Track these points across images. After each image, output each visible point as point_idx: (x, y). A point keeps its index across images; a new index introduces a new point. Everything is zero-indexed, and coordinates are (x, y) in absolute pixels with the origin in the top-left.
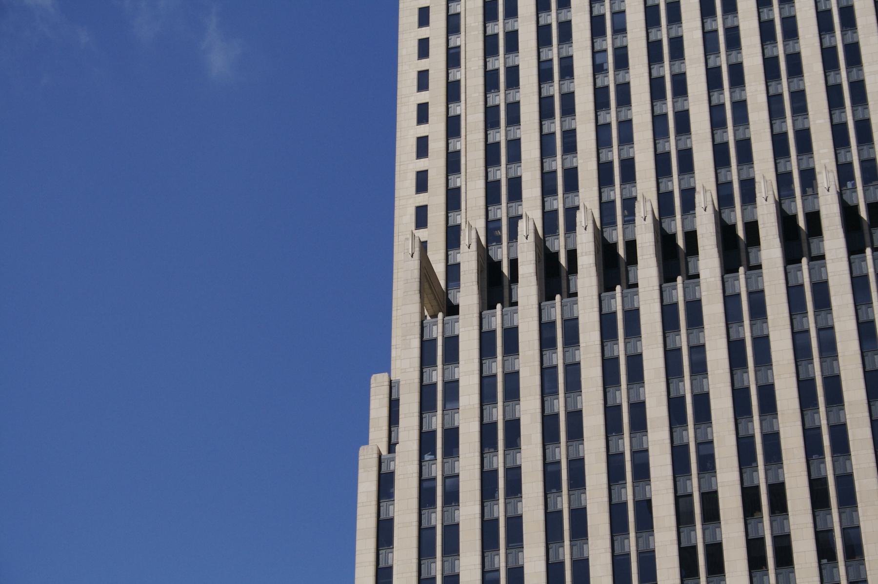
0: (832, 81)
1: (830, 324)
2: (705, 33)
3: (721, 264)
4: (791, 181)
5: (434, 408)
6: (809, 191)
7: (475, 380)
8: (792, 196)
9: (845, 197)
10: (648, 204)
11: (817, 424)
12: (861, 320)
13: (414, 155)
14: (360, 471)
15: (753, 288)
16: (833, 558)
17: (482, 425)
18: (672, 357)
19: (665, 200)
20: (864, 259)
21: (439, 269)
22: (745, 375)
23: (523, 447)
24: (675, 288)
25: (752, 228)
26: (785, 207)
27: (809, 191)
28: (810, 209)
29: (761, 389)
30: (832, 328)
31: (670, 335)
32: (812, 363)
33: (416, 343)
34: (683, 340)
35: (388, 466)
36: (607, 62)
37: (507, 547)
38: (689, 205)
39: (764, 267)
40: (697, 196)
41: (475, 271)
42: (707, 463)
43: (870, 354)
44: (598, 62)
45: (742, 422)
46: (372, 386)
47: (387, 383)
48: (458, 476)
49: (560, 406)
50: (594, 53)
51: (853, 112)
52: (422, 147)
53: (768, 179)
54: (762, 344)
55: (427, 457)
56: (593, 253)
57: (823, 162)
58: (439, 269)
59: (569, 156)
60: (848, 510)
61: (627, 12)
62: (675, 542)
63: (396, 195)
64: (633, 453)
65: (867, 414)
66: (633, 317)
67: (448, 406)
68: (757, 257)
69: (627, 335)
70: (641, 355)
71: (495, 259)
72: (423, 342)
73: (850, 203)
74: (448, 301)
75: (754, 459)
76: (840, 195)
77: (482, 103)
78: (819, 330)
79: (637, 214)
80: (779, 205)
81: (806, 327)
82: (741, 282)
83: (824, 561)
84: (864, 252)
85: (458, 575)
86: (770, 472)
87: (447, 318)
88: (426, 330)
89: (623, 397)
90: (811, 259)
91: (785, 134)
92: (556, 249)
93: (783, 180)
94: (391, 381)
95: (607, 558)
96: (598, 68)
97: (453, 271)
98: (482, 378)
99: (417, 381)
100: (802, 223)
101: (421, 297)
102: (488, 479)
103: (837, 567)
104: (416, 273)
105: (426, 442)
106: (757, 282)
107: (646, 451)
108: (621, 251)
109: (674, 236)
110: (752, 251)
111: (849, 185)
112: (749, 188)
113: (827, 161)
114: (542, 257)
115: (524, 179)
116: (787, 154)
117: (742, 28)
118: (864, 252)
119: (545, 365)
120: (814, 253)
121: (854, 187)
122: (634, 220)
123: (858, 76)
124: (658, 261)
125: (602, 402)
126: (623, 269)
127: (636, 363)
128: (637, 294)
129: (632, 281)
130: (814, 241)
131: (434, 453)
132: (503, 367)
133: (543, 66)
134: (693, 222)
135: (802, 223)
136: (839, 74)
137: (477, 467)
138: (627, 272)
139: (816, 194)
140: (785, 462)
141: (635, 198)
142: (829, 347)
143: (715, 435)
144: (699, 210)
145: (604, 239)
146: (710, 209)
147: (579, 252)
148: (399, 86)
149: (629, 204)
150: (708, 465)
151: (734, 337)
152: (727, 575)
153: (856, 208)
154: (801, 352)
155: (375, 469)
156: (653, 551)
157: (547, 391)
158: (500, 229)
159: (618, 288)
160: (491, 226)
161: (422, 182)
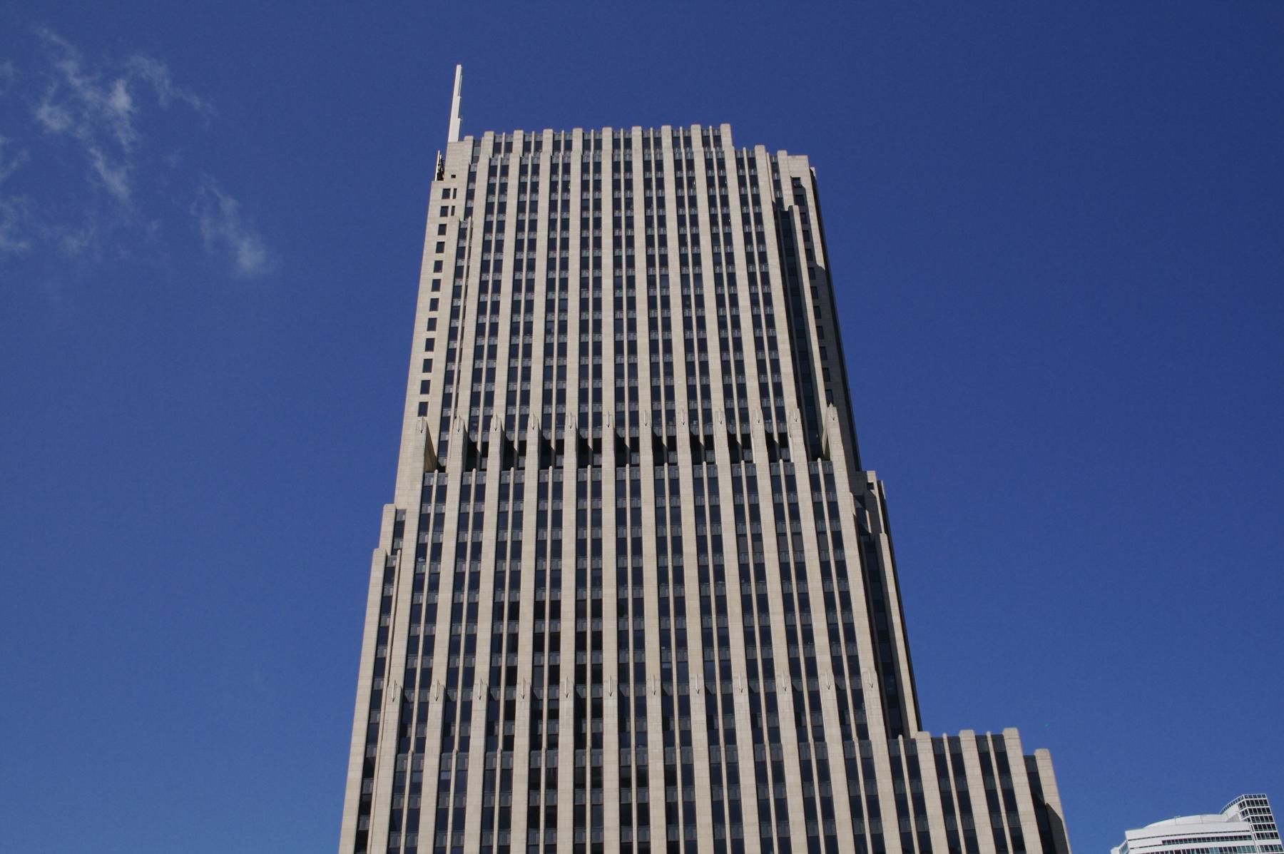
0: (689, 359)
1: (678, 504)
2: (615, 320)
3: (501, 463)
4: (660, 416)
5: (427, 530)
6: (671, 423)
7: (456, 514)
8: (660, 425)
9: (655, 430)
10: (462, 422)
11: (666, 564)
12: (697, 504)
13: (421, 369)
14: (373, 564)
15: (711, 476)
16: (669, 646)
17: (458, 544)
18: (502, 516)
19: (509, 419)
20: (702, 468)
21: (435, 442)
22: (505, 534)
23: (482, 560)
24: (586, 472)
25: (560, 443)
26: (618, 432)
27: (671, 423)
28: (559, 438)
29: (593, 541)
30: (679, 507)
31: (503, 503)
32: (586, 529)
33: (419, 487)
34: (510, 507)
35: (392, 563)
36: (553, 328)
37: (468, 622)
38: (524, 426)
39: (641, 465)
40: (529, 419)
41: (461, 446)
42: (556, 583)
43: (701, 525)
44: (548, 327)
45: (581, 560)
46: (384, 511)
47: (394, 511)
48: (439, 573)
49: (429, 539)
50: (546, 322)
51: (629, 381)
52: (428, 365)
53: (536, 415)
54: (637, 512)
55: (420, 560)
56: (537, 444)
57: (680, 407)
58: (435, 442)
59: (489, 384)
60: (680, 618)
61: (569, 300)
62: (532, 629)
63: (408, 393)
64: (431, 574)
65: (696, 562)
66: (481, 490)
67: (437, 529)
68: (561, 462)
69: (437, 501)
70: (561, 511)
71: (473, 441)
72: (424, 487)
73: (583, 436)
74: (438, 463)
75: (626, 582)
76: (615, 430)
77: (473, 343)
78: (671, 508)
79: (566, 424)
80: (578, 432)
81: (664, 505)
82: (472, 478)
83: (663, 648)
84: (625, 466)
85: (434, 636)
86: (635, 591)
87: (440, 474)
88: (427, 480)
89: (468, 537)
90: (593, 466)
91: (623, 388)
92: (476, 440)
93: (582, 418)
94: (396, 510)
95: (488, 636)
96: (548, 331)
97: (443, 445)
98: (460, 514)
99: (418, 511)
100: (590, 444)
101: (425, 459)
102: (458, 578)
103: (501, 657)
104: (423, 444)
105: (420, 550)
106: (636, 474)
107: (560, 570)
108: (479, 448)
109: (475, 444)
110: (559, 457)
111: (695, 422)
112: (561, 418)
113: (683, 407)
114: (466, 445)
115: (495, 393)
116: (623, 400)
117: (637, 320)
118: (548, 469)
119: (500, 511)
120: (595, 464)
121: (698, 424)
122: (564, 427)
123: (634, 360)
124: (463, 458)
125: (535, 537)
126: (553, 456)
127: (479, 517)
128: (523, 474)
129: (520, 466)
130: (596, 456)
131: (425, 557)
132: (435, 509)
133: (721, 319)
134: (525, 435)
135: (590, 444)
136: (588, 359)
137: (452, 569)
138: (481, 461)
139: (674, 426)
140: (645, 585)
141: (492, 416)
142: (676, 519)
143: (603, 565)
144: (492, 429)
145: (469, 439)
146: (536, 428)
147: (528, 442)
148: (416, 325)
149: (487, 419)
150: (598, 583)
151: (619, 506)
152: (519, 653)
153: (661, 438)
154: (660, 520)
155: (383, 564)
156: (559, 633)
157: (500, 526)
158: (478, 422)
159: (474, 470)
160: (472, 420)
161: (425, 387)
